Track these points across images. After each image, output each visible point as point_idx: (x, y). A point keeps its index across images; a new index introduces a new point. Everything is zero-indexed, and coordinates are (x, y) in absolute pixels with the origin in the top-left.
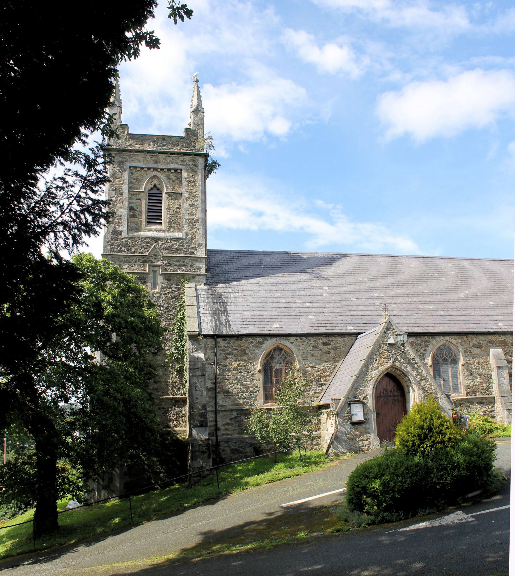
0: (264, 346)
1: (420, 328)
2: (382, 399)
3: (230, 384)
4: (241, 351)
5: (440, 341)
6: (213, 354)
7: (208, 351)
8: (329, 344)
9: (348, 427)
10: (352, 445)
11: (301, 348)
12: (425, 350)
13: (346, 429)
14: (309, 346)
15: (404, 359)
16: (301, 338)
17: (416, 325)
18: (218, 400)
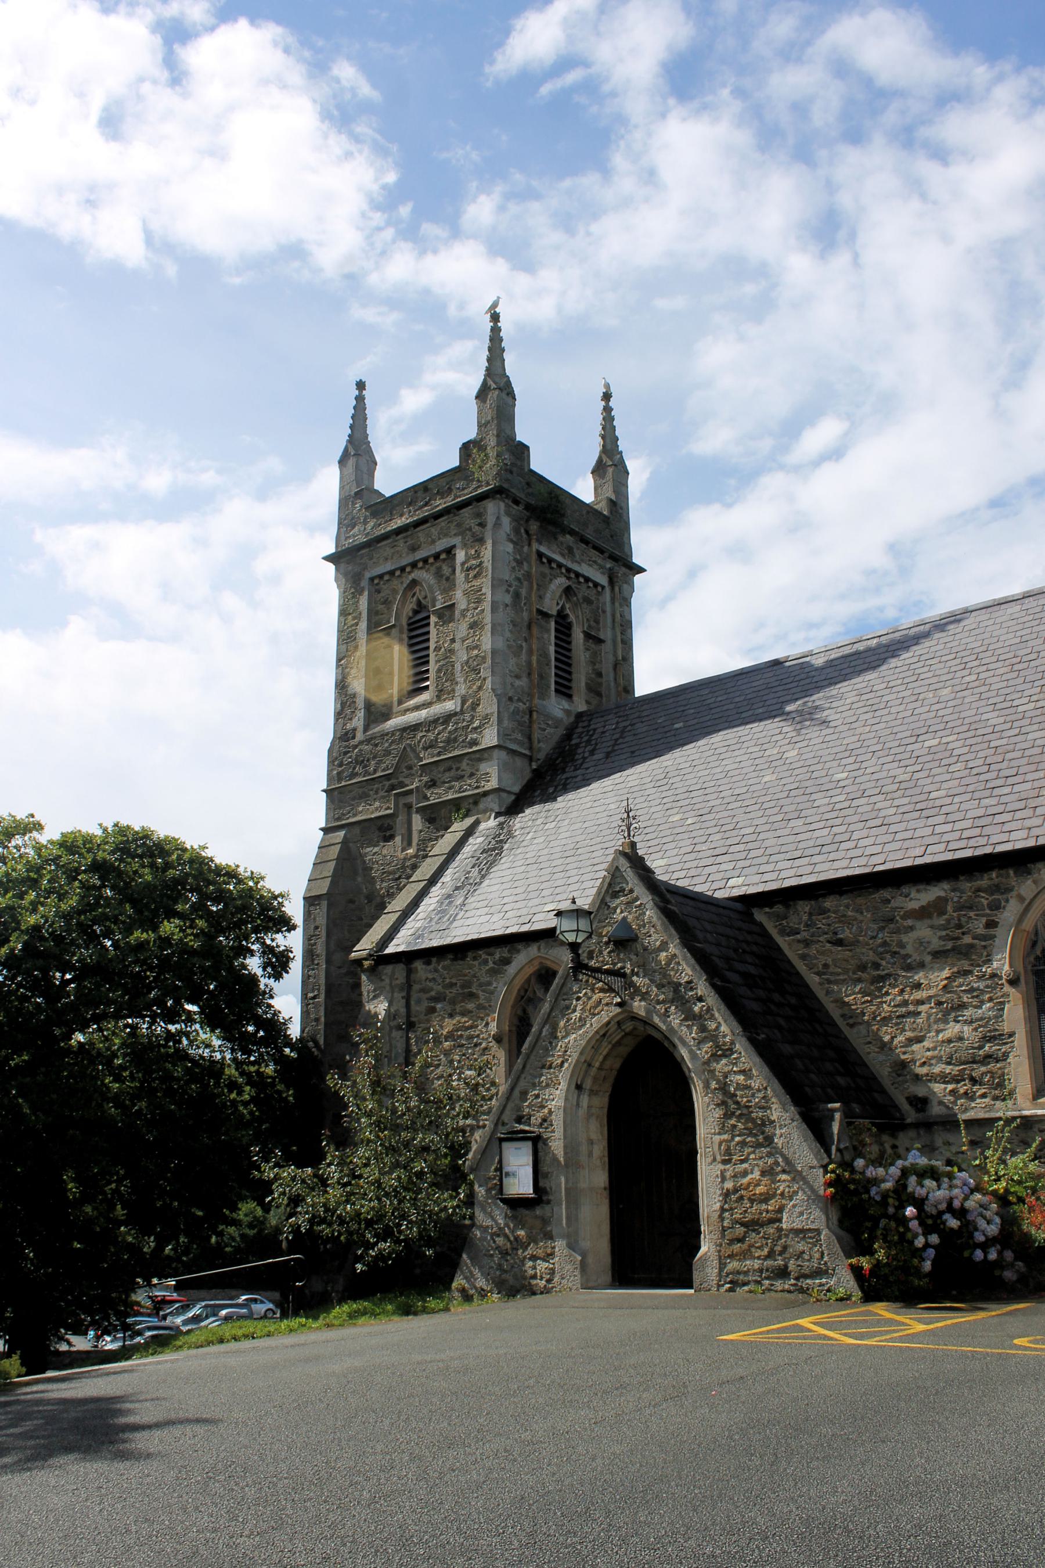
0: (511, 970)
7: (396, 995)
10: (505, 1271)
13: (493, 1219)
15: (660, 986)
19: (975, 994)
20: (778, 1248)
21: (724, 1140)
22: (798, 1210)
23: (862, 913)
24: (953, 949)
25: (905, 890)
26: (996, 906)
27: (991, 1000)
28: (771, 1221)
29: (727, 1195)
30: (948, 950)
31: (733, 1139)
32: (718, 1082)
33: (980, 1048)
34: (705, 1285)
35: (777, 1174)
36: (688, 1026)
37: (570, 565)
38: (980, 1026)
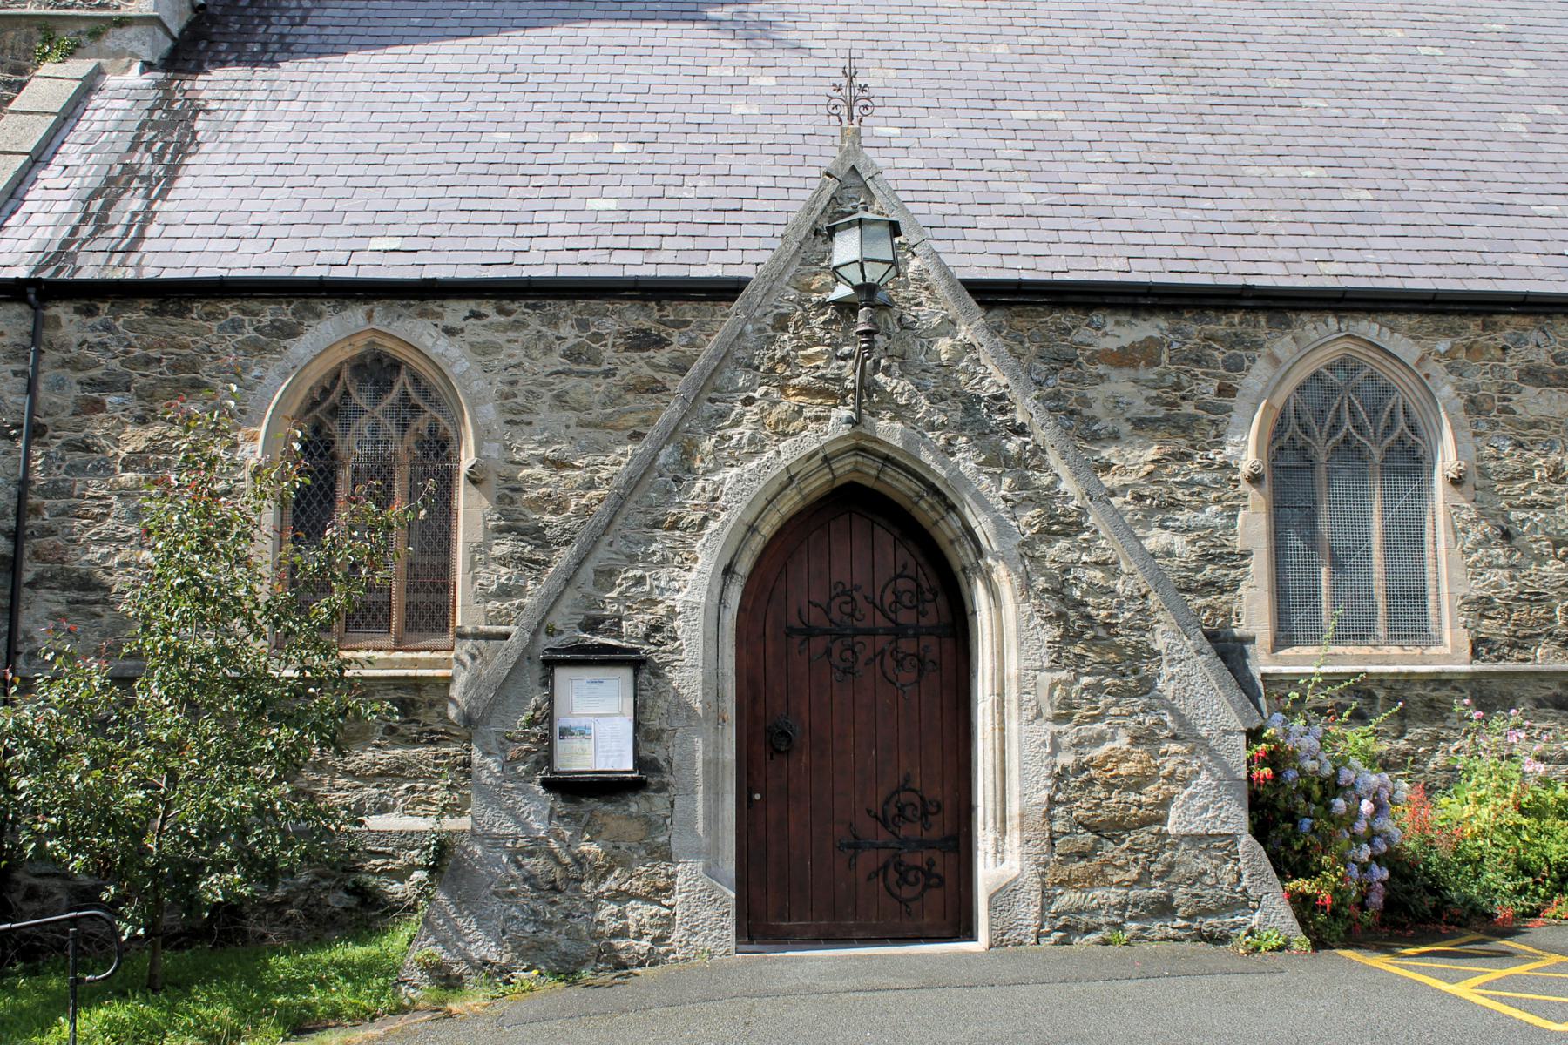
1: (1201, 266)
2: (818, 644)
3: (101, 542)
4: (175, 368)
5: (1318, 343)
6: (21, 382)
8: (660, 343)
9: (536, 811)
10: (549, 925)
11: (501, 359)
12: (1226, 391)
13: (518, 820)
14: (549, 349)
16: (506, 304)
17: (1183, 252)
18: (24, 622)
19: (1195, 489)
20: (1157, 868)
21: (1060, 682)
22: (1198, 802)
23: (1021, 343)
24: (1167, 419)
25: (1097, 317)
26: (1236, 366)
27: (1218, 501)
28: (1145, 823)
29: (1060, 777)
30: (1159, 420)
31: (1076, 680)
32: (1050, 578)
33: (1198, 570)
34: (1011, 935)
35: (1161, 742)
36: (992, 475)
38: (1200, 538)
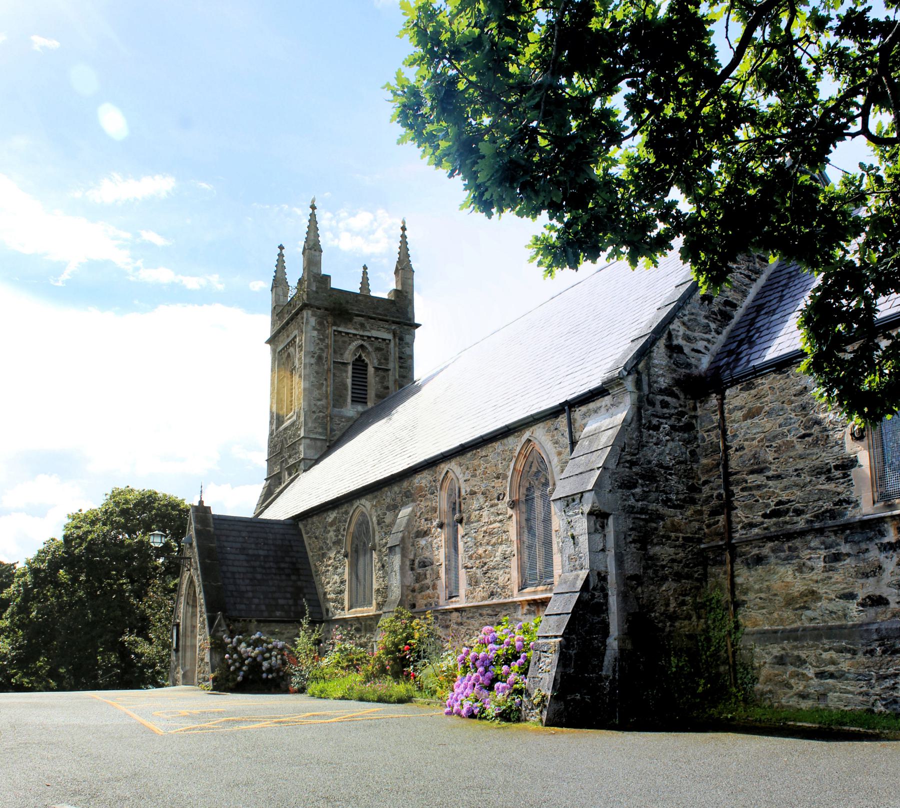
37: (361, 333)
